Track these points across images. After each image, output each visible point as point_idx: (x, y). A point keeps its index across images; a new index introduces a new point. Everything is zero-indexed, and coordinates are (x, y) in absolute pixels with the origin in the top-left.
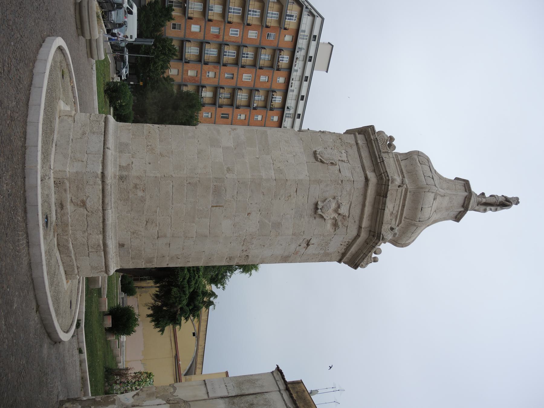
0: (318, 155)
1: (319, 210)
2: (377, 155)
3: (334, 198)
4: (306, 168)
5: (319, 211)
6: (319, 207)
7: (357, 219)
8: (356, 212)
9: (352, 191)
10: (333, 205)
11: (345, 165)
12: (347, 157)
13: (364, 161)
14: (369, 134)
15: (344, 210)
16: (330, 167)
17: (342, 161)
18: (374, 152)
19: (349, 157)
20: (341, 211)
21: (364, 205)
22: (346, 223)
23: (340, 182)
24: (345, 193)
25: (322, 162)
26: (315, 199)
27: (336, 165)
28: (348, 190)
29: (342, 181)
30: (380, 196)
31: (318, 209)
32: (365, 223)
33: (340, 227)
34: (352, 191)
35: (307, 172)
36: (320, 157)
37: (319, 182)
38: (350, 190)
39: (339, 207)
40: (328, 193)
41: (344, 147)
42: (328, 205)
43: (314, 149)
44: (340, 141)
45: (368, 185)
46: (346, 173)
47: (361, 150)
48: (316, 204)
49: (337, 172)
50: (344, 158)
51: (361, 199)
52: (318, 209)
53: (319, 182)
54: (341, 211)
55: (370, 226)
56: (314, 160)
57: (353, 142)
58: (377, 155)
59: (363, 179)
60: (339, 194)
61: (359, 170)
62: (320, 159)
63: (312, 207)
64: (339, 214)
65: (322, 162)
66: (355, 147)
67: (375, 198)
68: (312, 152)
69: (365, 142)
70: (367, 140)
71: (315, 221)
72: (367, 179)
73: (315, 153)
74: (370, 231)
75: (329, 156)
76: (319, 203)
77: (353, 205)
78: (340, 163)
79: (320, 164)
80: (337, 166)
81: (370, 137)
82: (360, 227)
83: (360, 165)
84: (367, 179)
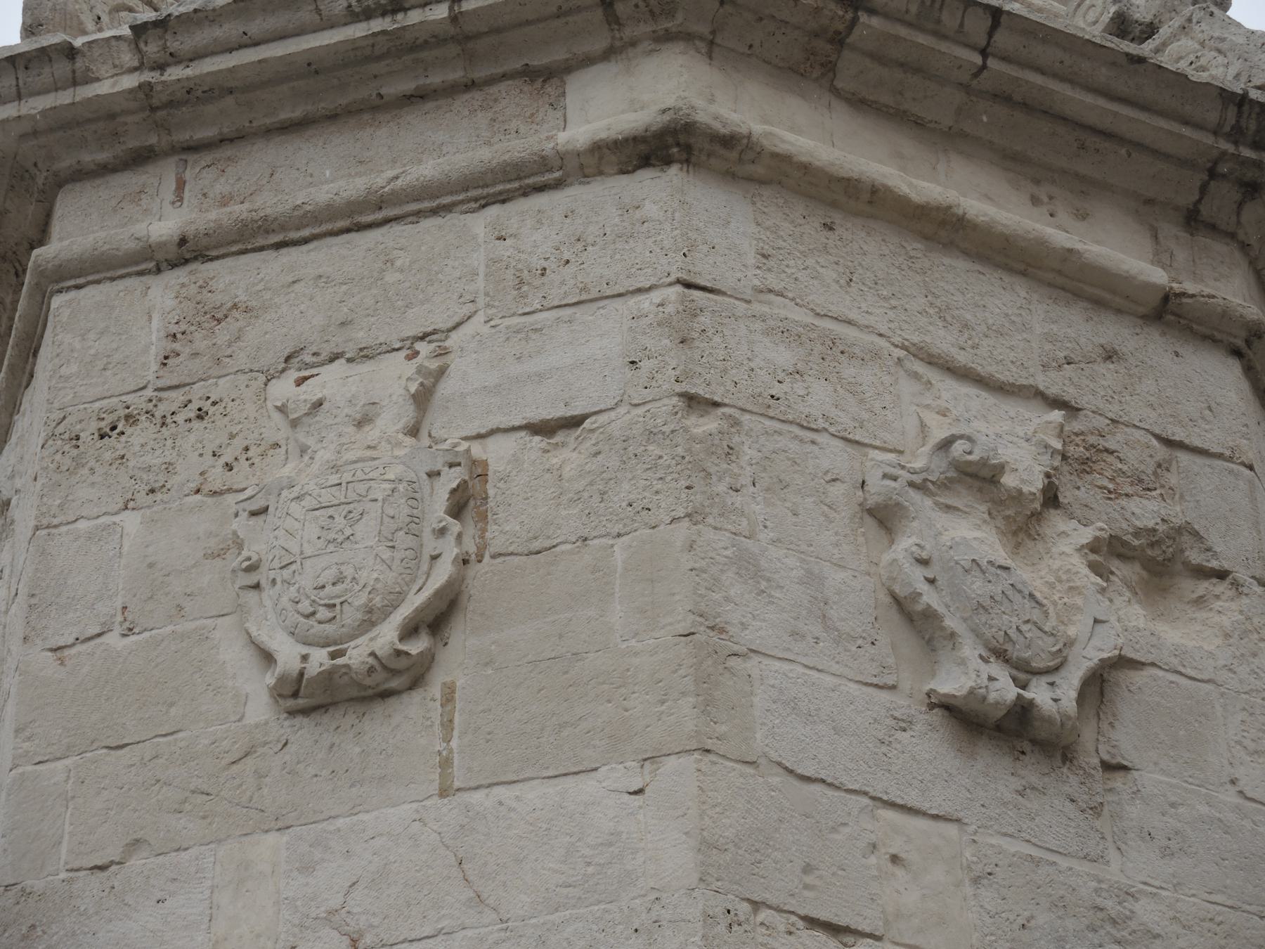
0: (357, 655)
1: (1039, 693)
2: (358, 31)
3: (884, 517)
4: (533, 794)
5: (1055, 697)
6: (1004, 690)
7: (1080, 329)
8: (1016, 326)
9: (799, 315)
10: (969, 533)
11: (468, 373)
12: (365, 355)
13: (428, 170)
14: (65, 124)
15: (1021, 444)
16: (507, 528)
17: (422, 398)
18: (312, 69)
19: (360, 336)
20: (1025, 471)
21: (942, 230)
22: (1137, 452)
23: (707, 425)
24: (817, 397)
25: (437, 619)
26: (905, 725)
27: (480, 471)
28: (785, 357)
29: (692, 401)
30: (839, 41)
31: (1023, 711)
32: (1118, 247)
33: (1177, 513)
34: (799, 315)
35: (587, 786)
36: (386, 636)
37: (713, 648)
38: (785, 332)
39: (980, 478)
40: (836, 577)
41: (222, 388)
42: (977, 587)
43: (260, 708)
44: (139, 436)
45: (728, 141)
46: (587, 358)
47: (270, 203)
48: (967, 721)
49: (570, 455)
50: (393, 378)
51: (873, 249)
52: (1023, 711)
53: (713, 648)
54: (1025, 471)
55: (1144, 208)
56: (415, 711)
57: (163, 295)
58: (358, 31)
59: (656, 190)
60: (833, 455)
61: (536, 226)
62: (410, 631)
63: (990, 780)
64: (1051, 498)
65: (437, 619)
66: (231, 277)
67: (859, 103)
68: (304, 733)
69: (163, 176)
70: (141, 158)
71: (1149, 778)
72: (664, 147)
73: (309, 698)
74: (1193, 220)
75: (366, 531)
76: (952, 683)
77: (944, 341)
78: (449, 427)
79: (463, 640)
80: (497, 453)
81: (106, 115)
82: (1165, 312)
83: (480, 223)
84: (664, 147)
